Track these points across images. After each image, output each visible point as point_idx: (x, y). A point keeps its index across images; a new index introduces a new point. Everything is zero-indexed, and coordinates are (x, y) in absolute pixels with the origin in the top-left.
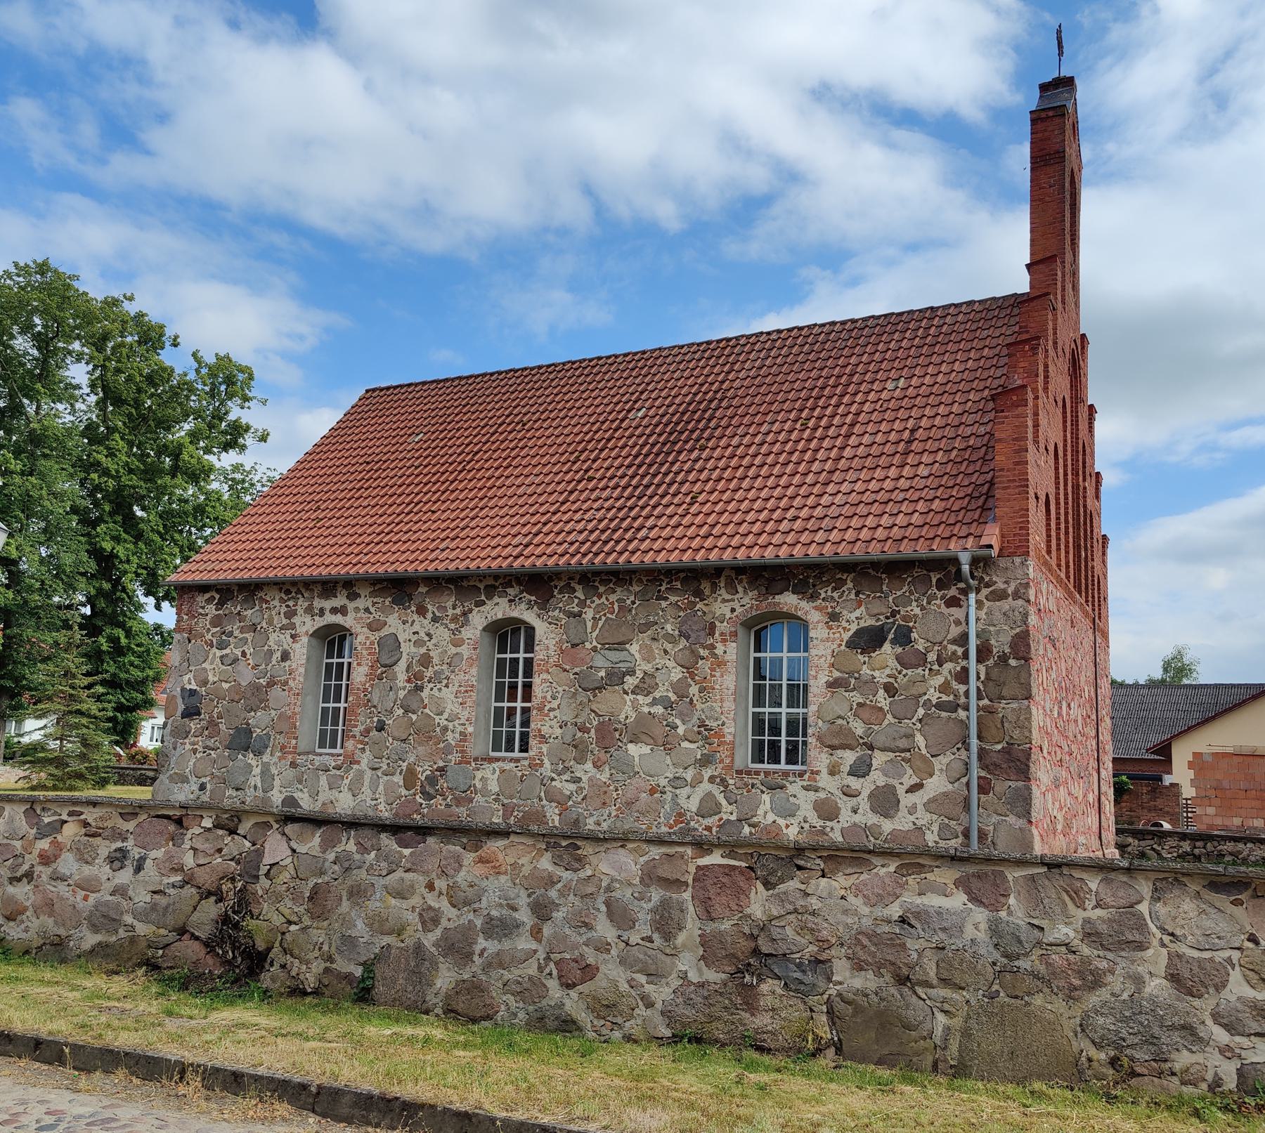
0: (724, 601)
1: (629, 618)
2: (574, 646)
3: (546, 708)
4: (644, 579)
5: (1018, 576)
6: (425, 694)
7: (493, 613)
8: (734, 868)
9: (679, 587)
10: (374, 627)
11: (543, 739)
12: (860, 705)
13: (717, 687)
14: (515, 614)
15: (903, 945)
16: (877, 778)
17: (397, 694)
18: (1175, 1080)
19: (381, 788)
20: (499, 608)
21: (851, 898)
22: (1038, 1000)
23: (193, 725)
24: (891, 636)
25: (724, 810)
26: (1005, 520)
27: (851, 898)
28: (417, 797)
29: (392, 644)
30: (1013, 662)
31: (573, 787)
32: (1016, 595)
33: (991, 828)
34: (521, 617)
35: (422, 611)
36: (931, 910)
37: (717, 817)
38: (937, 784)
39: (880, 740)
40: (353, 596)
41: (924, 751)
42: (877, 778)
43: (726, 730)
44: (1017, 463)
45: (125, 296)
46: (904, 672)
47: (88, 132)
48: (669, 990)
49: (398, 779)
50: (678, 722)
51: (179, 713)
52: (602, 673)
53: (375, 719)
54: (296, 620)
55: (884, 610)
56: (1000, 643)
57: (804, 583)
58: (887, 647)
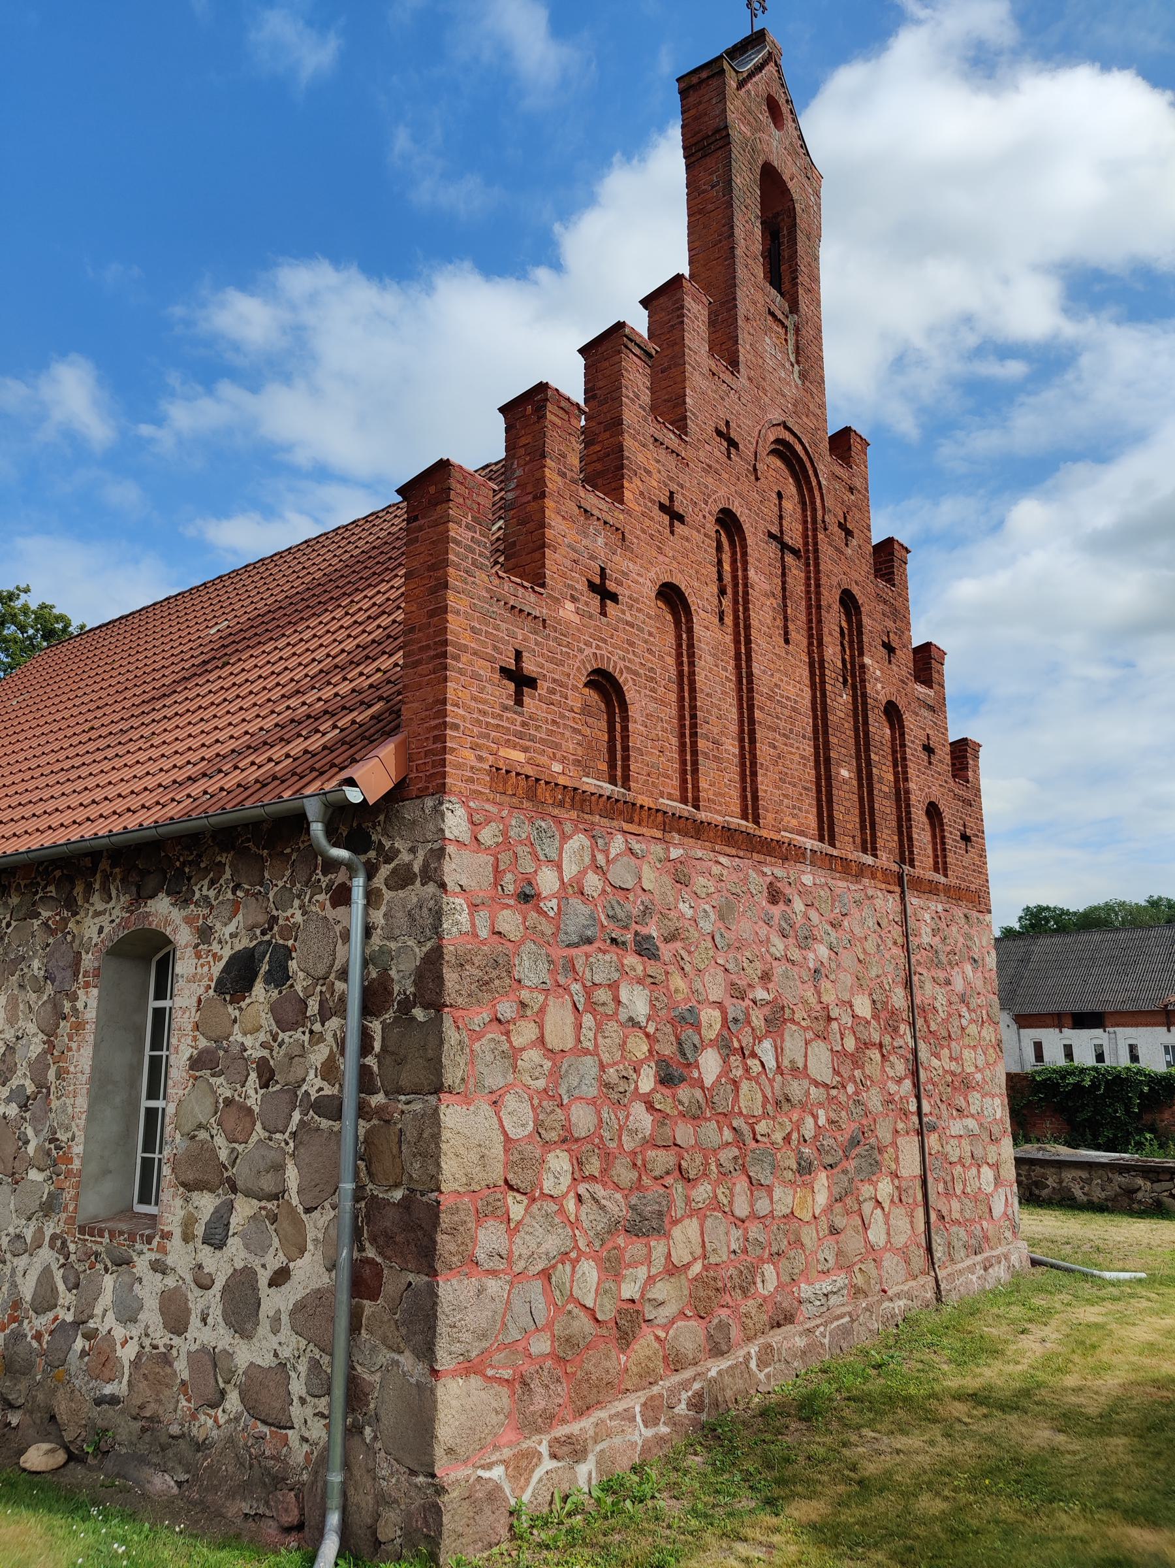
0: (97, 914)
4: (22, 883)
9: (54, 894)
12: (229, 1102)
13: (72, 1069)
24: (265, 967)
25: (61, 1301)
30: (419, 1013)
33: (377, 1377)
39: (241, 1173)
41: (295, 1201)
44: (432, 614)
45: (18, 588)
46: (281, 1036)
50: (30, 1133)
56: (402, 982)
58: (259, 989)
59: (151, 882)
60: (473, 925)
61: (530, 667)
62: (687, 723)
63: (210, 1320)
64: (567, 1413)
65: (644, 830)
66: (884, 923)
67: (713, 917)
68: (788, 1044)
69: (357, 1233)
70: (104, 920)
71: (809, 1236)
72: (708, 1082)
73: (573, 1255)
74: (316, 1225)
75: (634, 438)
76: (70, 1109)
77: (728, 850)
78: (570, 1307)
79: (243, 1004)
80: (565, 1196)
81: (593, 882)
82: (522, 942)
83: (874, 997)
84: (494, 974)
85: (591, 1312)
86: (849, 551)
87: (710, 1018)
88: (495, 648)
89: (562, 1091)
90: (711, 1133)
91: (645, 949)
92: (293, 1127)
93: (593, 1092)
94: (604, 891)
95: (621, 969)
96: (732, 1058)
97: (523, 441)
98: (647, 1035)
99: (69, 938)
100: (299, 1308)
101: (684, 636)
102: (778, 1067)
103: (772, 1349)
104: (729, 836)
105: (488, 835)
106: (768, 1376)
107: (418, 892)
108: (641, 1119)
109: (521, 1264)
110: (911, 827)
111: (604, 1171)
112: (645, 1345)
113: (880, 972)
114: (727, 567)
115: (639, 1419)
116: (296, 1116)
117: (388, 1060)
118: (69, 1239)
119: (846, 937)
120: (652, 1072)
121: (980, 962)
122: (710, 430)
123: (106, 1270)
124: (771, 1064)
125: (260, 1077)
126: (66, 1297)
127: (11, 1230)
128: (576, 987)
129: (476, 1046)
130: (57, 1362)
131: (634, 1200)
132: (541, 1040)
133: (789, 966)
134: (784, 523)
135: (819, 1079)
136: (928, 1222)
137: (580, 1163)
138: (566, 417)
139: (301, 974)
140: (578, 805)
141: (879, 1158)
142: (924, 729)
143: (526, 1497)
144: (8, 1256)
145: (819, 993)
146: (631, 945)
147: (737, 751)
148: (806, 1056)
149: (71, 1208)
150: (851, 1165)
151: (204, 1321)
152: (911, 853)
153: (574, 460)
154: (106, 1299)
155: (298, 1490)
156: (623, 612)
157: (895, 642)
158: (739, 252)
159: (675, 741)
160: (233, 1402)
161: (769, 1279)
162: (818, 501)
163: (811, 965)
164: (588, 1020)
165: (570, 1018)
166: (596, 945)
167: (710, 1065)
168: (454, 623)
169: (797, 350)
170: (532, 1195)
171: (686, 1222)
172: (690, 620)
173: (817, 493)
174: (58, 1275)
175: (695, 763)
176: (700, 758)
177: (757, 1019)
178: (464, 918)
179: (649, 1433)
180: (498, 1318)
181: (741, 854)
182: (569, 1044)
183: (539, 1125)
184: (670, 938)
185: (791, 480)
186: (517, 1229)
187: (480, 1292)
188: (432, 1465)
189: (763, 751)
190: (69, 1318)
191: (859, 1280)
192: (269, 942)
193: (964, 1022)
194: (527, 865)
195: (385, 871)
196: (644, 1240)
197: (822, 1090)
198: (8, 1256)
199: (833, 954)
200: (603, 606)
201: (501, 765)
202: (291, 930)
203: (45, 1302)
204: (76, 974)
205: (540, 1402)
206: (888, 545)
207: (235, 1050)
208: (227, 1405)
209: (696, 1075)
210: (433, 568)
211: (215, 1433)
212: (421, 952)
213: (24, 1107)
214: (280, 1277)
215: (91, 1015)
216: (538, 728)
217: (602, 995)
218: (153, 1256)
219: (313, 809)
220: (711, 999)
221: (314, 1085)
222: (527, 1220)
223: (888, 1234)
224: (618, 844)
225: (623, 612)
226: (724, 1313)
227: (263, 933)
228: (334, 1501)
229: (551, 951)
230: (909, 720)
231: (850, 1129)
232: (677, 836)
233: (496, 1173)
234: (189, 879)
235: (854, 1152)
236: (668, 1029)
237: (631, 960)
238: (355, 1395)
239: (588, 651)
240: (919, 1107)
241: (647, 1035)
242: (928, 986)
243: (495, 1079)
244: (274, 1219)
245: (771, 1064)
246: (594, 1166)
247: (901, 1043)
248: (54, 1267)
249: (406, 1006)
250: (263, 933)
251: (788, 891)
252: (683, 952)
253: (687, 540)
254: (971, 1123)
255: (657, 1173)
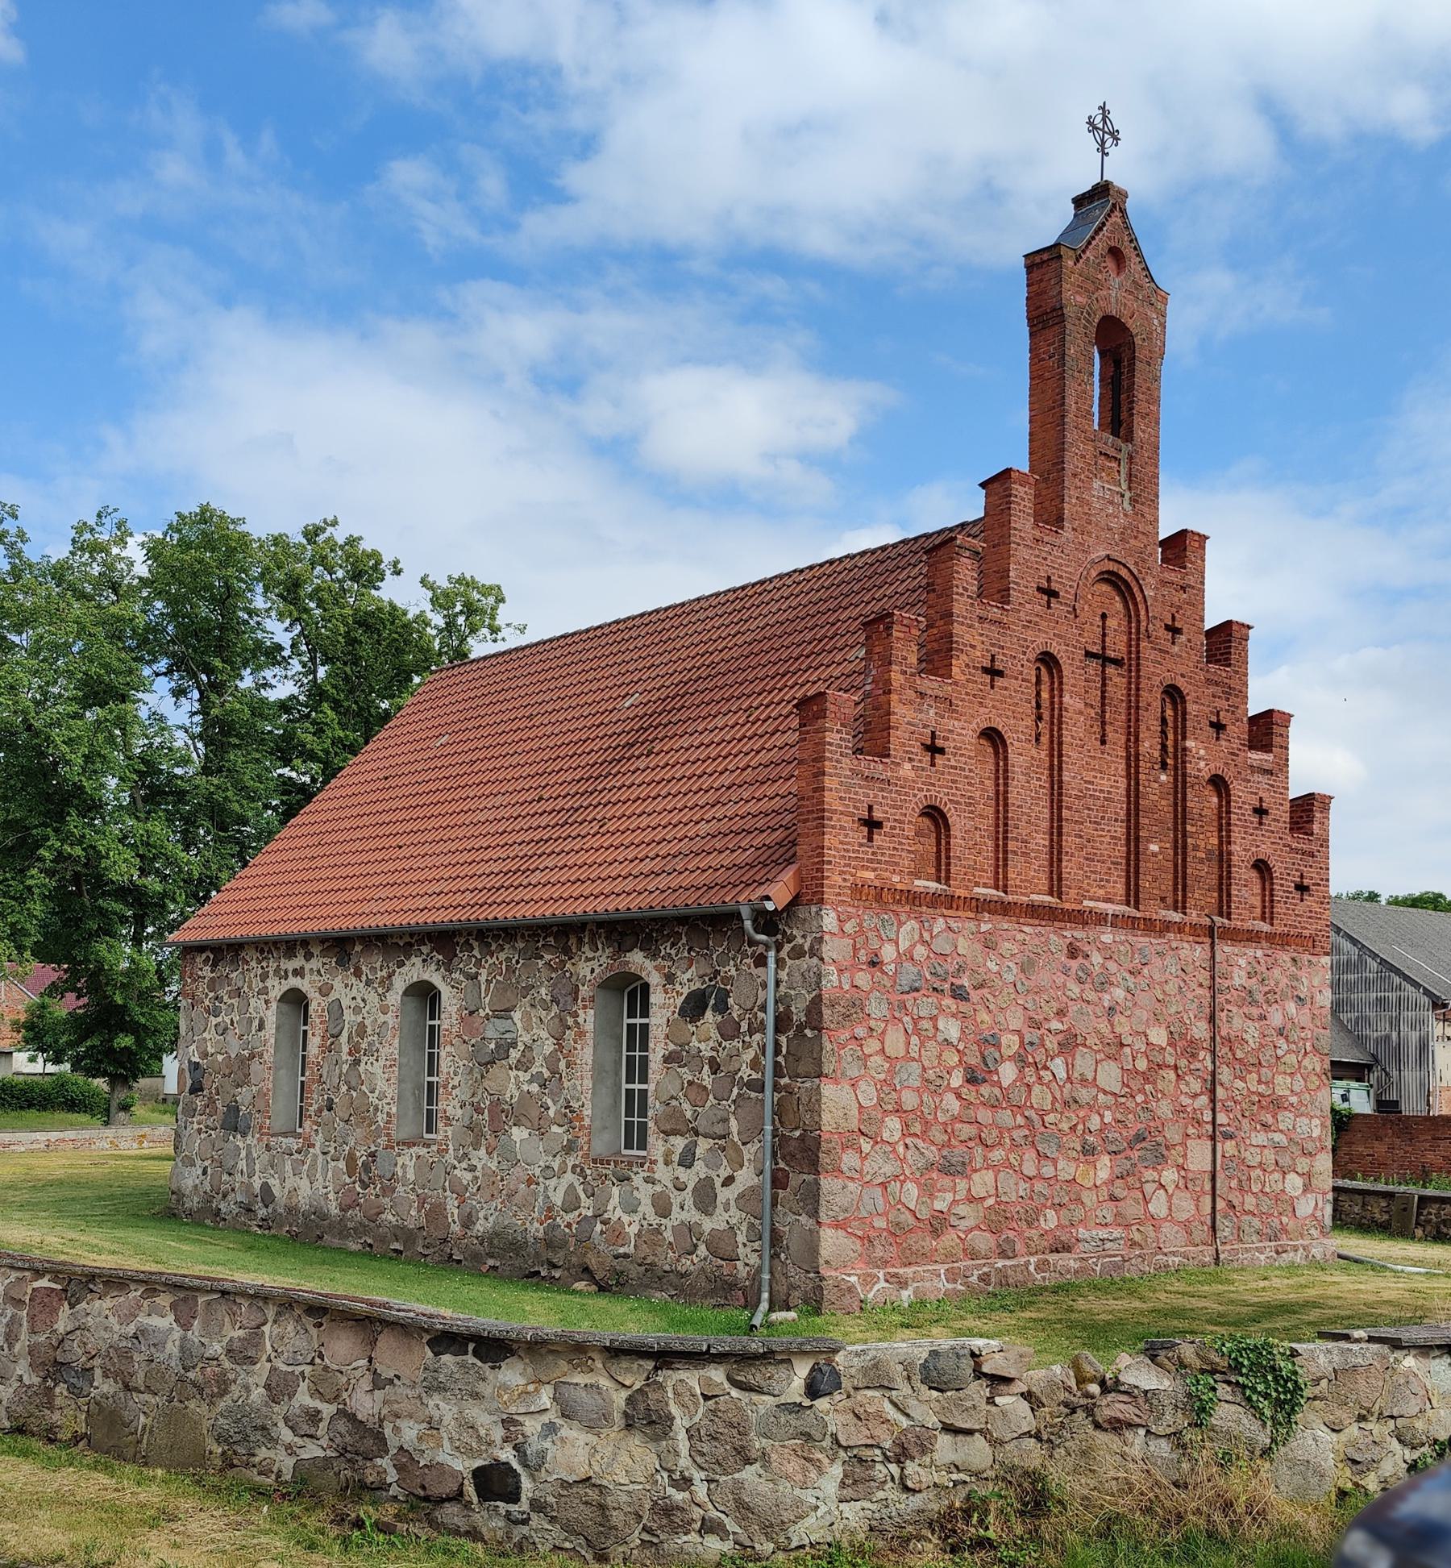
0: (588, 960)
1: (514, 980)
2: (471, 1013)
3: (450, 1086)
4: (526, 934)
5: (814, 929)
6: (362, 1068)
7: (410, 975)
8: (53, 1290)
10: (325, 991)
11: (448, 1120)
12: (690, 1083)
13: (578, 1062)
14: (426, 977)
15: (132, 1357)
16: (700, 1169)
17: (341, 1068)
18: (255, 1471)
19: (330, 1174)
20: (415, 970)
21: (111, 1318)
22: (192, 1405)
23: (199, 1103)
24: (712, 1002)
25: (583, 1204)
26: (804, 861)
27: (111, 1318)
28: (356, 1185)
29: (337, 1009)
30: (808, 1032)
31: (469, 1176)
32: (813, 952)
33: (787, 1228)
34: (430, 980)
35: (358, 973)
36: (150, 1328)
37: (577, 1213)
38: (746, 1177)
39: (702, 1124)
40: (308, 956)
41: (736, 1139)
42: (700, 1169)
43: (586, 1113)
44: (815, 790)
45: (325, 521)
46: (724, 1043)
47: (493, 186)
48: (11, 1390)
49: (342, 1165)
50: (550, 1102)
51: (187, 1090)
52: (492, 1046)
53: (326, 1097)
54: (269, 983)
55: (709, 972)
56: (798, 1014)
57: (649, 937)
58: (709, 1014)
59: (629, 940)
60: (840, 982)
61: (878, 815)
62: (1001, 829)
63: (686, 1207)
64: (897, 1262)
65: (960, 913)
66: (1189, 969)
67: (1015, 971)
68: (1078, 1061)
69: (774, 1154)
70: (594, 964)
71: (1089, 1198)
72: (1005, 1084)
73: (902, 1178)
74: (749, 1152)
75: (962, 624)
76: (579, 1087)
77: (1031, 921)
78: (899, 1207)
79: (698, 1024)
80: (897, 1143)
81: (920, 951)
82: (871, 991)
83: (1172, 1029)
84: (853, 1011)
85: (913, 1212)
86: (1176, 649)
87: (1011, 1044)
88: (855, 807)
89: (896, 1081)
90: (1005, 1117)
91: (959, 994)
92: (733, 1096)
93: (917, 1084)
94: (928, 957)
95: (940, 1008)
96: (1027, 1069)
97: (877, 650)
98: (958, 1051)
99: (568, 975)
100: (741, 1196)
101: (1001, 764)
102: (1068, 1078)
103: (1049, 1263)
104: (1034, 912)
105: (849, 927)
106: (1044, 1278)
107: (806, 962)
108: (952, 1104)
109: (868, 1178)
110: (1230, 885)
111: (924, 1132)
112: (949, 1239)
113: (1181, 1009)
114: (1045, 695)
115: (943, 1276)
116: (735, 1091)
117: (791, 1058)
118: (586, 1167)
119: (1143, 983)
120: (961, 1075)
121: (1309, 1001)
122: (1032, 591)
123: (614, 1184)
124: (1062, 1074)
125: (711, 1068)
126: (585, 1201)
127: (542, 1164)
128: (906, 1019)
129: (842, 1052)
130: (583, 1239)
131: (945, 1153)
132: (883, 1050)
133: (1084, 1005)
134: (1107, 639)
135: (1107, 1089)
136: (1214, 1208)
137: (907, 1125)
138: (907, 630)
139: (736, 1007)
140: (911, 901)
141: (1165, 1153)
142: (1256, 794)
143: (870, 1296)
144: (541, 1180)
145: (1112, 1025)
146: (948, 992)
147: (1047, 843)
148: (1096, 1071)
149: (585, 1148)
150: (1135, 1155)
151: (682, 1208)
152: (1229, 907)
153: (913, 659)
154: (615, 1200)
155: (744, 1290)
156: (949, 760)
157: (1225, 718)
158: (1070, 418)
159: (990, 843)
160: (702, 1250)
161: (1050, 1220)
162: (1142, 612)
163: (1106, 1005)
164: (914, 1040)
165: (902, 1038)
166: (922, 992)
167: (1008, 1073)
168: (828, 797)
169: (1130, 478)
170: (875, 1140)
171: (984, 1172)
172: (1006, 751)
173: (1141, 606)
174: (580, 1189)
175: (1006, 859)
176: (1010, 856)
177: (1051, 1043)
178: (834, 978)
179: (950, 1286)
180: (855, 1203)
181: (1044, 923)
182: (902, 1053)
183: (880, 1100)
184: (980, 986)
185: (1117, 598)
186: (866, 1158)
187: (843, 1188)
188: (818, 1267)
189: (1069, 842)
190: (590, 1213)
191: (1137, 1237)
192: (715, 986)
193: (1280, 1053)
194: (875, 944)
195: (787, 947)
196: (952, 1178)
197: (1110, 1097)
198: (541, 1180)
199: (1129, 997)
200: (933, 758)
201: (858, 882)
202: (728, 980)
203: (571, 1204)
204: (576, 999)
205: (879, 1252)
206: (1226, 631)
207: (694, 1052)
208: (698, 1252)
209: (996, 1079)
210: (816, 775)
211: (692, 1268)
212: (809, 997)
213: (543, 1085)
214: (729, 1181)
215: (589, 1027)
216: (883, 854)
217: (925, 1024)
218: (646, 1174)
219: (745, 912)
220: (1011, 1028)
221: (746, 1073)
222: (872, 1153)
223: (1170, 1209)
224: (940, 924)
225: (949, 760)
226: (1011, 1234)
227: (710, 980)
228: (766, 1287)
229: (890, 996)
230: (1237, 789)
231: (1134, 1127)
232: (987, 915)
233: (854, 1124)
234: (657, 941)
235: (1139, 1146)
236: (975, 1047)
237: (948, 1002)
238: (776, 1238)
239: (921, 795)
240: (1214, 1118)
241: (958, 1051)
242: (1237, 1022)
243: (853, 1072)
244: (724, 1149)
245: (1062, 1074)
246: (917, 1128)
247: (1199, 1065)
248: (576, 1184)
249: (801, 1028)
250: (710, 980)
251: (1086, 948)
252: (989, 996)
253: (1006, 689)
254: (1278, 1137)
255: (962, 1138)
